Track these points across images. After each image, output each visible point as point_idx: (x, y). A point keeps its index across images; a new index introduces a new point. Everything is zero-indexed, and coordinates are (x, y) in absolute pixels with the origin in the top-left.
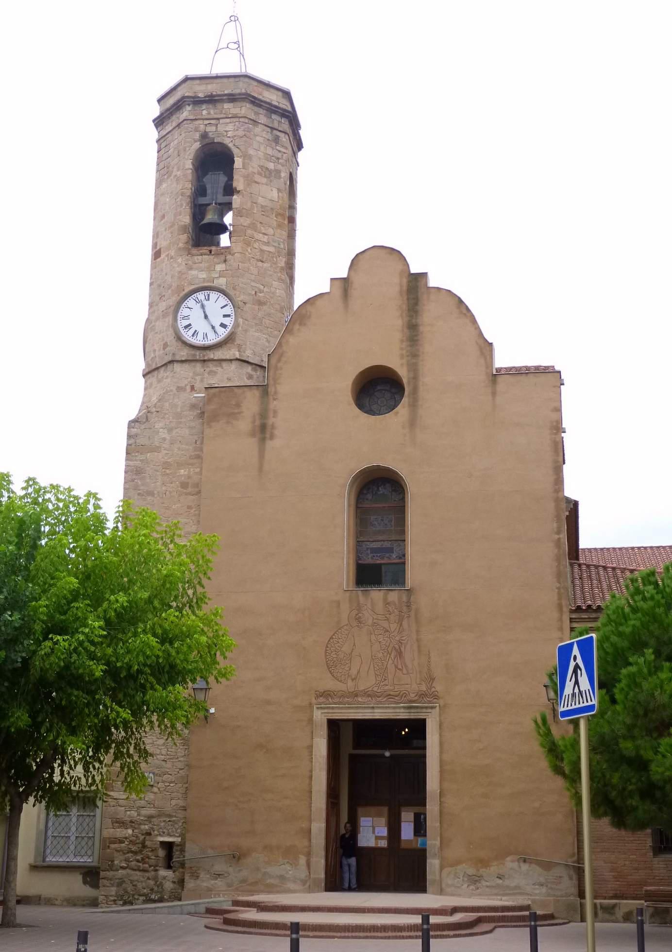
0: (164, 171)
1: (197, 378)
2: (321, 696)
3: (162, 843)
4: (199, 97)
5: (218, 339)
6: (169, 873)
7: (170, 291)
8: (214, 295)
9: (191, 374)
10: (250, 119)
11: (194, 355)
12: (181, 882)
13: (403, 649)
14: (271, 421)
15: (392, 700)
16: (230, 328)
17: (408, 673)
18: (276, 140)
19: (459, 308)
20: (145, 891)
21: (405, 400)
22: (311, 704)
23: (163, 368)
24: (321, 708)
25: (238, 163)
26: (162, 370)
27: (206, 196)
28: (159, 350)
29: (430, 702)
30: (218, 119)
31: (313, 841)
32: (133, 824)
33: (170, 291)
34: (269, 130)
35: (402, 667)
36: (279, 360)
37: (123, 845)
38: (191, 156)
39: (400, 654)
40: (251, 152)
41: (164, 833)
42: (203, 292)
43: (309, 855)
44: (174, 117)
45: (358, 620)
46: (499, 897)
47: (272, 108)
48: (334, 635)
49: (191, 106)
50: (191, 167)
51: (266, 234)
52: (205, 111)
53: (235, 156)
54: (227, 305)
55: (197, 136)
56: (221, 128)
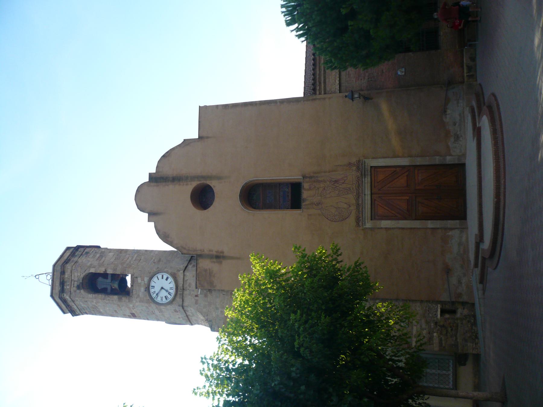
0: (95, 311)
1: (192, 293)
2: (359, 224)
3: (441, 315)
4: (60, 290)
5: (173, 282)
6: (459, 311)
7: (150, 308)
8: (152, 284)
9: (190, 297)
10: (74, 264)
11: (180, 294)
12: (464, 304)
13: (334, 180)
14: (214, 253)
15: (361, 185)
16: (168, 275)
17: (347, 177)
18: (87, 253)
19: (166, 157)
20: (469, 326)
21: (208, 182)
22: (363, 230)
23: (187, 312)
24: (365, 223)
25: (92, 270)
26: (188, 313)
27: (107, 288)
28: (178, 315)
29: (362, 164)
30: (72, 280)
31: (438, 226)
32: (431, 332)
33: (150, 308)
34: (82, 256)
35: (343, 180)
36: (185, 249)
37: (443, 338)
38: (87, 294)
39: (336, 181)
40: (89, 264)
41: (435, 314)
42: (150, 289)
43: (446, 229)
44: (70, 304)
45: (318, 204)
46: (466, 124)
47: (72, 254)
48: (326, 217)
49: (64, 294)
50: (92, 295)
51: (129, 258)
52: (67, 287)
53: (89, 272)
54: (157, 277)
55: (78, 291)
56: (76, 279)
